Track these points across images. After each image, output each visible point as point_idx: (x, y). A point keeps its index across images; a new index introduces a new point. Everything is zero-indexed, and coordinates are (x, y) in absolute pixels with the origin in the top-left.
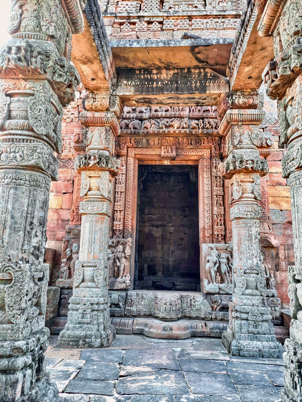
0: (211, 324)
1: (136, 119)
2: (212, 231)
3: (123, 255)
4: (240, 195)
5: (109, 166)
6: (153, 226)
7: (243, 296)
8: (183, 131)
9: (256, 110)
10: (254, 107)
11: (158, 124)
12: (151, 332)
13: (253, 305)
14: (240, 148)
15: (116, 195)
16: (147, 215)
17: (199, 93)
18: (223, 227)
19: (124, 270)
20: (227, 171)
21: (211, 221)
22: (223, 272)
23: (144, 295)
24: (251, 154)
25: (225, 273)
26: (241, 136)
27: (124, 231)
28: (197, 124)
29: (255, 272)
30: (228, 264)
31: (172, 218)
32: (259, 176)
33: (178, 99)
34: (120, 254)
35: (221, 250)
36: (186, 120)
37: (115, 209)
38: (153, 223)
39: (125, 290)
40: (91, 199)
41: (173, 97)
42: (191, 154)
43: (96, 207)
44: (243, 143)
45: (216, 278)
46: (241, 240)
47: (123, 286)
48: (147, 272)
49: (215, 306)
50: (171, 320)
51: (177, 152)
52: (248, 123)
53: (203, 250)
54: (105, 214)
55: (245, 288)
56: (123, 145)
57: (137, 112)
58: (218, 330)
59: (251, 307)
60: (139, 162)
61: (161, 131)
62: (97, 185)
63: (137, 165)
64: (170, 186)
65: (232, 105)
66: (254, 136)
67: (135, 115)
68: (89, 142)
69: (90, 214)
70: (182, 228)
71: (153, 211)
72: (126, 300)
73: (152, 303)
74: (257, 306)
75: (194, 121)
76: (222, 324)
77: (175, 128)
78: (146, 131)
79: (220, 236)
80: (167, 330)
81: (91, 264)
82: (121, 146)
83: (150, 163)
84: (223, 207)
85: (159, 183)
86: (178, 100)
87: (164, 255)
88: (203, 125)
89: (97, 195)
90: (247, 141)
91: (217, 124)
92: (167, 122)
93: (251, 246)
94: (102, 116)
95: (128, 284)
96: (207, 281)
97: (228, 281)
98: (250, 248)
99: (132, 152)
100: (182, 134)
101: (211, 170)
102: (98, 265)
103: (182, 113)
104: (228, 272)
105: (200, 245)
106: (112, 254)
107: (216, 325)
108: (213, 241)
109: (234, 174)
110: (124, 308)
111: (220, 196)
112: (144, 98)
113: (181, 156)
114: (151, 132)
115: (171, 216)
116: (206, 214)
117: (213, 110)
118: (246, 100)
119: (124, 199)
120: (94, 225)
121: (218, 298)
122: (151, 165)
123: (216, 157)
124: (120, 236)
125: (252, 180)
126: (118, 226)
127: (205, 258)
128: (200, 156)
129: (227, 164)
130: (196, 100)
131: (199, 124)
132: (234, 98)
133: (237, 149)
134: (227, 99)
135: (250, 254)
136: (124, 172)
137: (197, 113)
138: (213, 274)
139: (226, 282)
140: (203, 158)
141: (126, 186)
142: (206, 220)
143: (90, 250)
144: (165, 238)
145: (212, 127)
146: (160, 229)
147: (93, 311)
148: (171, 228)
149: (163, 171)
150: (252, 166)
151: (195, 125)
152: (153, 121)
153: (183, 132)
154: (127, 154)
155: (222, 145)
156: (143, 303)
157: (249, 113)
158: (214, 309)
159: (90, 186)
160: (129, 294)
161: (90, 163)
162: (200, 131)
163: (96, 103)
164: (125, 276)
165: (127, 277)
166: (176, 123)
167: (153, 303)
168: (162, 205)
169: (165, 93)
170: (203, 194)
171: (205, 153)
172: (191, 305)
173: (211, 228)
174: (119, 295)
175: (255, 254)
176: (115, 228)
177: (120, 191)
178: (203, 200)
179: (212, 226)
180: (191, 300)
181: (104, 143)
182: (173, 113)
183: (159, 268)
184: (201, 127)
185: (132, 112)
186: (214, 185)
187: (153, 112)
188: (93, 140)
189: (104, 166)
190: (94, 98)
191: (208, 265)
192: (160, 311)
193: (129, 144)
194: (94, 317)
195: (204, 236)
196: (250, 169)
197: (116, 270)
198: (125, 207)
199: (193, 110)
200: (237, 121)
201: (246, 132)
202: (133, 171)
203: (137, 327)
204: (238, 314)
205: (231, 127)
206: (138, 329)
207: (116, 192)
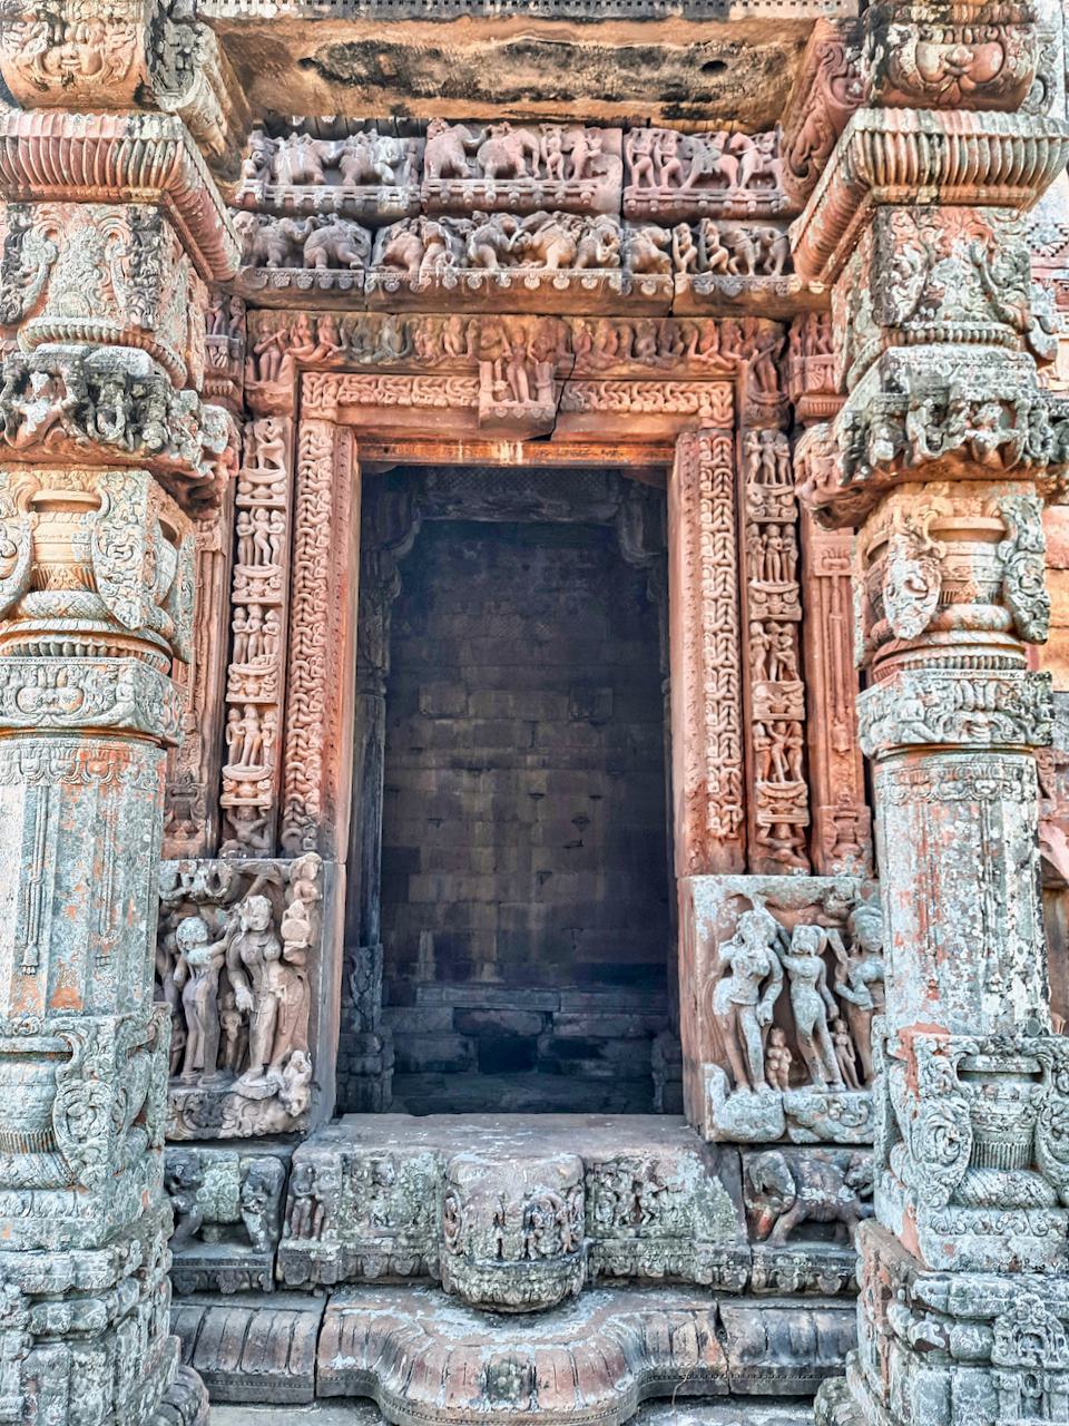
0: (749, 1322)
1: (344, 214)
2: (745, 806)
3: (272, 949)
4: (931, 610)
5: (152, 435)
6: (456, 765)
7: (955, 1211)
8: (590, 280)
9: (1020, 117)
10: (1000, 94)
11: (459, 243)
12: (413, 1403)
13: (1015, 1268)
14: (927, 340)
15: (237, 624)
16: (431, 718)
17: (685, 17)
18: (800, 784)
19: (276, 1032)
20: (851, 469)
21: (737, 759)
22: (805, 1026)
23: (385, 1167)
24: (991, 372)
25: (816, 1032)
26: (928, 266)
27: (281, 816)
28: (666, 247)
29: (1026, 1065)
30: (831, 982)
31: (542, 730)
32: (1033, 500)
33: (566, 55)
34: (255, 941)
35: (790, 908)
36: (607, 223)
37: (231, 698)
38: (455, 752)
39: (288, 1136)
40: (40, 639)
41: (535, 40)
42: (636, 407)
43: (70, 691)
44: (942, 312)
45: (767, 1058)
46: (934, 876)
47: (271, 1117)
48: (433, 967)
49: (767, 1213)
50: (534, 1312)
51: (560, 394)
52: (968, 190)
53: (699, 911)
54: (128, 729)
55: (962, 1164)
56: (275, 354)
57: (349, 179)
58: (785, 1360)
59: (1004, 1285)
60: (361, 450)
61: (476, 275)
62: (77, 554)
63: (352, 469)
64: (531, 591)
65: (879, 83)
66: (1002, 269)
67: (334, 193)
68: (29, 294)
69: (32, 731)
70: (581, 774)
71: (457, 699)
72: (283, 1198)
73: (430, 1205)
74: (1039, 1270)
75: (646, 230)
76: (805, 1317)
77: (552, 264)
78: (393, 276)
79: (784, 831)
80: (507, 1388)
81: (36, 1044)
82: (263, 360)
83: (420, 455)
84: (798, 684)
85: (482, 577)
86: (564, 65)
87: (506, 890)
88: (693, 250)
89: (80, 616)
90: (965, 296)
91: (765, 248)
92: (509, 232)
93: (999, 914)
94: (108, 134)
95: (296, 1109)
96: (720, 1075)
97: (829, 1071)
98: (991, 922)
99: (323, 396)
100: (587, 296)
101: (735, 490)
102: (76, 1047)
103: (586, 187)
104: (832, 1027)
105: (682, 882)
106: (210, 942)
107: (773, 1329)
108: (746, 857)
109: (887, 490)
110: (275, 1244)
111: (782, 623)
112: (369, 49)
113: (583, 419)
114: (425, 281)
115: (535, 723)
116: (711, 718)
117: (746, 176)
118: (961, 52)
119: (278, 645)
120: (55, 800)
121: (784, 1171)
122: (440, 469)
123: (764, 422)
124: (256, 840)
125: (997, 525)
126: (246, 789)
127: (712, 950)
128: (678, 420)
129: (855, 428)
130: (666, 71)
131: (676, 249)
132: (893, 38)
133: (906, 343)
134: (849, 52)
135: (994, 959)
136: (281, 500)
137: (665, 187)
138: (754, 1041)
139: (821, 1076)
140: (697, 430)
141: (292, 574)
142: (712, 750)
143: (29, 954)
144: (508, 817)
145: (742, 266)
146: (486, 781)
147: (40, 1339)
148: (534, 775)
149: (497, 518)
150: (1001, 435)
151: (655, 252)
152: (431, 227)
153: (589, 284)
154: (299, 405)
155: (796, 359)
156: (378, 1207)
157: (976, 130)
158: (762, 1229)
159: (34, 559)
160: (299, 1167)
161: (22, 418)
162: (682, 282)
163: (67, 50)
164: (284, 1064)
165: (291, 1071)
166: (556, 240)
167: (434, 1206)
168: (494, 673)
169: (489, 8)
170: (697, 617)
171: (705, 402)
172: (637, 1207)
173: (738, 796)
174: (246, 1175)
175: (1021, 960)
176: (228, 800)
177: (256, 598)
178: (697, 645)
179: (744, 782)
180: (637, 1184)
181: (122, 302)
182: (539, 186)
183: (483, 945)
184: (683, 262)
185: (318, 176)
186: (754, 566)
187: (432, 178)
188: (57, 280)
189: (113, 433)
190: (52, 19)
191: (726, 991)
192: (470, 1260)
193: (304, 350)
194: (47, 1382)
195: (703, 836)
196: (993, 456)
197: (232, 1030)
198: (287, 684)
199: (643, 175)
200: (908, 181)
201: (958, 247)
202: (327, 496)
203: (340, 1362)
204: (928, 1330)
205: (871, 218)
206: (349, 1374)
207: (234, 606)
